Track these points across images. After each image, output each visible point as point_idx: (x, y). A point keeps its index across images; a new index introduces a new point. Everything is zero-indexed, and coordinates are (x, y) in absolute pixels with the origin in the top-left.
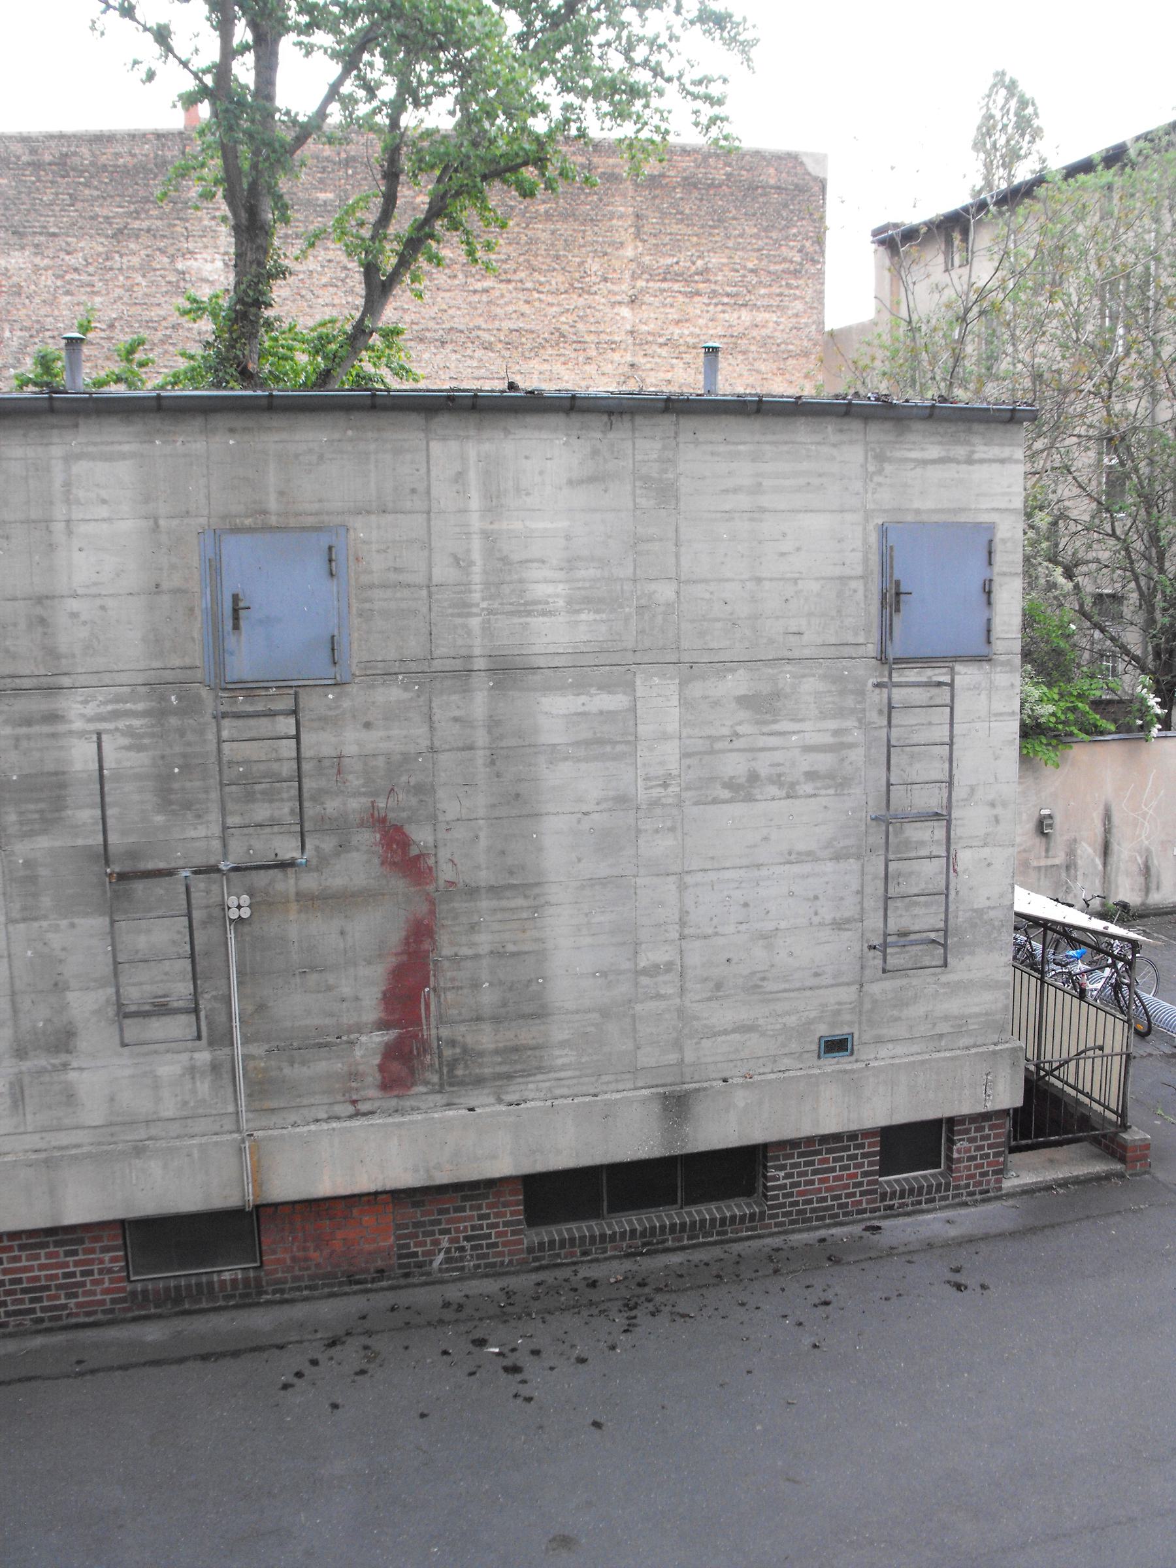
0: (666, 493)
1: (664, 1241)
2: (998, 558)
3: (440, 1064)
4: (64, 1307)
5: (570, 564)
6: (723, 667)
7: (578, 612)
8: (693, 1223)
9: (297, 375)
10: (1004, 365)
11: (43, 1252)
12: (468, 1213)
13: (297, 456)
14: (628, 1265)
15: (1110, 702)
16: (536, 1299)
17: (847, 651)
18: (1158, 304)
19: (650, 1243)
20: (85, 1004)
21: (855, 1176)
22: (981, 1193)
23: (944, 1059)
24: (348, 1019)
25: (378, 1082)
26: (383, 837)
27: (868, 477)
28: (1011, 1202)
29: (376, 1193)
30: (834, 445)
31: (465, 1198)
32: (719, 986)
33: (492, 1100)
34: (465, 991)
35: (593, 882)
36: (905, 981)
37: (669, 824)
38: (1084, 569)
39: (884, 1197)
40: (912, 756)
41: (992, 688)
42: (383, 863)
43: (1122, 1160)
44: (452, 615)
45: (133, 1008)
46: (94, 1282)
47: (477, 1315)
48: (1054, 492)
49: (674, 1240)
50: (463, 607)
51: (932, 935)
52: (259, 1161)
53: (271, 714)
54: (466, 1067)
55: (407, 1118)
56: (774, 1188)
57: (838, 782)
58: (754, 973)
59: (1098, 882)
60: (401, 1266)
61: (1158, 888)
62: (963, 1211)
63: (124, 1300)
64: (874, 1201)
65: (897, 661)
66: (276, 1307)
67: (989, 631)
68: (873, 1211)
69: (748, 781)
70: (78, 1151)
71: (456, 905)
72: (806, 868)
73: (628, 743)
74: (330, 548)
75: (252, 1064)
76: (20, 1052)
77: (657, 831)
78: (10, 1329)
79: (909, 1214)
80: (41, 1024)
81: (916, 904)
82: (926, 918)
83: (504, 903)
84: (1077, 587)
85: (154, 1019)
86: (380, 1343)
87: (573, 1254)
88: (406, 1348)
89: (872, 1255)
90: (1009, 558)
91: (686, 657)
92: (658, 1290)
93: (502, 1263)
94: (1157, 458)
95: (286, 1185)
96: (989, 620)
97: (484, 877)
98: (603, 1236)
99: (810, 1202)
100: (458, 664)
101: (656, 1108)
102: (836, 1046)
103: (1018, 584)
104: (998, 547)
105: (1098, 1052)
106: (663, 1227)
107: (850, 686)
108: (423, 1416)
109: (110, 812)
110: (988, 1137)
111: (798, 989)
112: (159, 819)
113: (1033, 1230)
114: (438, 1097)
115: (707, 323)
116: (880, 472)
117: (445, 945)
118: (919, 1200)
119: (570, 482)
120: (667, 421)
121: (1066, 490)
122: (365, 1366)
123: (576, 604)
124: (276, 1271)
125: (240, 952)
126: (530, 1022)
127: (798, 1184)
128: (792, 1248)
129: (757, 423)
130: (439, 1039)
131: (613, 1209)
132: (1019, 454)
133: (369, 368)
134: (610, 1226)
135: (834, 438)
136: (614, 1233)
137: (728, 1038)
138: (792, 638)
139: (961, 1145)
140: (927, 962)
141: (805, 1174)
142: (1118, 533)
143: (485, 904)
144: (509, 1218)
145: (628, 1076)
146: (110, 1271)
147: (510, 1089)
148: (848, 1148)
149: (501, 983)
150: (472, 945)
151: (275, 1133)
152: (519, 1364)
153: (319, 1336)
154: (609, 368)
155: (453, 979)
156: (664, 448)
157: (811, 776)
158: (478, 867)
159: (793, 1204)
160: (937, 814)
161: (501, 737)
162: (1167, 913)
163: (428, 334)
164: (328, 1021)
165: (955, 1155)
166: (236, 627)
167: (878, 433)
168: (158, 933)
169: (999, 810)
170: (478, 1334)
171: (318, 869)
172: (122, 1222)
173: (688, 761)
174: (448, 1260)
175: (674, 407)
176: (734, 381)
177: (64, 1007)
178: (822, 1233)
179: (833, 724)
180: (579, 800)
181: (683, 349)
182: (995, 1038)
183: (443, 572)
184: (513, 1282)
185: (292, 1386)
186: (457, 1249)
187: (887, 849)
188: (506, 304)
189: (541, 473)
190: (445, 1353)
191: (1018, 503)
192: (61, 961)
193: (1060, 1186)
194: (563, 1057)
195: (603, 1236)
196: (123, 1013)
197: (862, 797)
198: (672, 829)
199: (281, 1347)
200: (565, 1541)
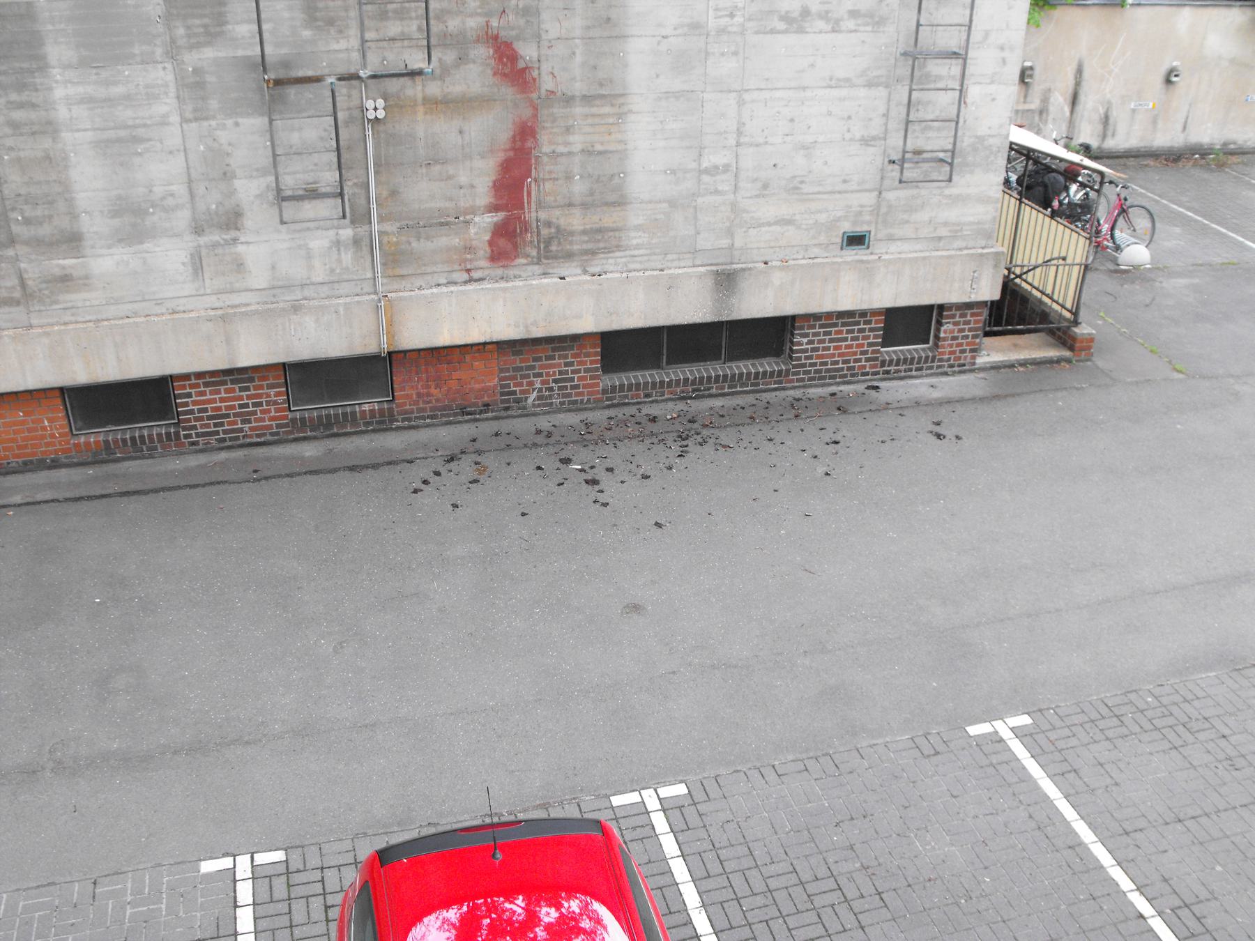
3: (539, 242)
4: (241, 430)
8: (733, 376)
11: (222, 388)
14: (681, 406)
19: (699, 390)
20: (250, 190)
21: (863, 345)
22: (959, 366)
25: (488, 255)
26: (496, 52)
28: (982, 375)
29: (485, 344)
32: (765, 186)
33: (579, 271)
34: (560, 182)
35: (668, 95)
36: (915, 192)
37: (733, 48)
39: (883, 364)
42: (495, 74)
43: (1071, 349)
45: (289, 193)
46: (263, 412)
47: (563, 440)
51: (941, 155)
55: (510, 284)
56: (798, 351)
57: (876, 20)
59: (1064, 127)
61: (1113, 135)
62: (944, 379)
63: (286, 425)
64: (875, 366)
66: (406, 432)
69: (801, 15)
70: (249, 308)
71: (555, 110)
72: (844, 92)
75: (385, 239)
76: (198, 230)
77: (723, 54)
78: (201, 446)
80: (214, 206)
81: (930, 128)
82: (937, 141)
83: (594, 110)
85: (306, 202)
86: (488, 460)
87: (638, 396)
89: (873, 408)
92: (705, 426)
93: (582, 400)
95: (414, 336)
97: (579, 88)
99: (825, 364)
101: (710, 282)
102: (856, 240)
105: (1061, 262)
109: (265, 27)
110: (968, 323)
112: (307, 34)
113: (997, 397)
114: (536, 267)
117: (546, 143)
118: (912, 367)
124: (404, 404)
125: (377, 146)
127: (816, 349)
130: (538, 221)
134: (668, 375)
139: (947, 327)
140: (935, 176)
141: (823, 341)
143: (579, 110)
146: (275, 403)
148: (858, 323)
149: (590, 176)
150: (567, 144)
151: (405, 294)
155: (550, 172)
158: (573, 79)
159: (812, 365)
160: (955, 53)
162: (1117, 157)
164: (448, 204)
165: (942, 335)
168: (308, 130)
169: (1006, 54)
170: (563, 455)
171: (441, 78)
172: (284, 364)
174: (539, 398)
177: (232, 193)
178: (833, 389)
180: (660, 25)
182: (983, 243)
184: (591, 416)
187: (912, 81)
190: (539, 468)
192: (228, 154)
193: (1021, 365)
194: (636, 238)
196: (282, 198)
197: (894, 35)
198: (735, 53)
199: (410, 462)
200: (636, 608)
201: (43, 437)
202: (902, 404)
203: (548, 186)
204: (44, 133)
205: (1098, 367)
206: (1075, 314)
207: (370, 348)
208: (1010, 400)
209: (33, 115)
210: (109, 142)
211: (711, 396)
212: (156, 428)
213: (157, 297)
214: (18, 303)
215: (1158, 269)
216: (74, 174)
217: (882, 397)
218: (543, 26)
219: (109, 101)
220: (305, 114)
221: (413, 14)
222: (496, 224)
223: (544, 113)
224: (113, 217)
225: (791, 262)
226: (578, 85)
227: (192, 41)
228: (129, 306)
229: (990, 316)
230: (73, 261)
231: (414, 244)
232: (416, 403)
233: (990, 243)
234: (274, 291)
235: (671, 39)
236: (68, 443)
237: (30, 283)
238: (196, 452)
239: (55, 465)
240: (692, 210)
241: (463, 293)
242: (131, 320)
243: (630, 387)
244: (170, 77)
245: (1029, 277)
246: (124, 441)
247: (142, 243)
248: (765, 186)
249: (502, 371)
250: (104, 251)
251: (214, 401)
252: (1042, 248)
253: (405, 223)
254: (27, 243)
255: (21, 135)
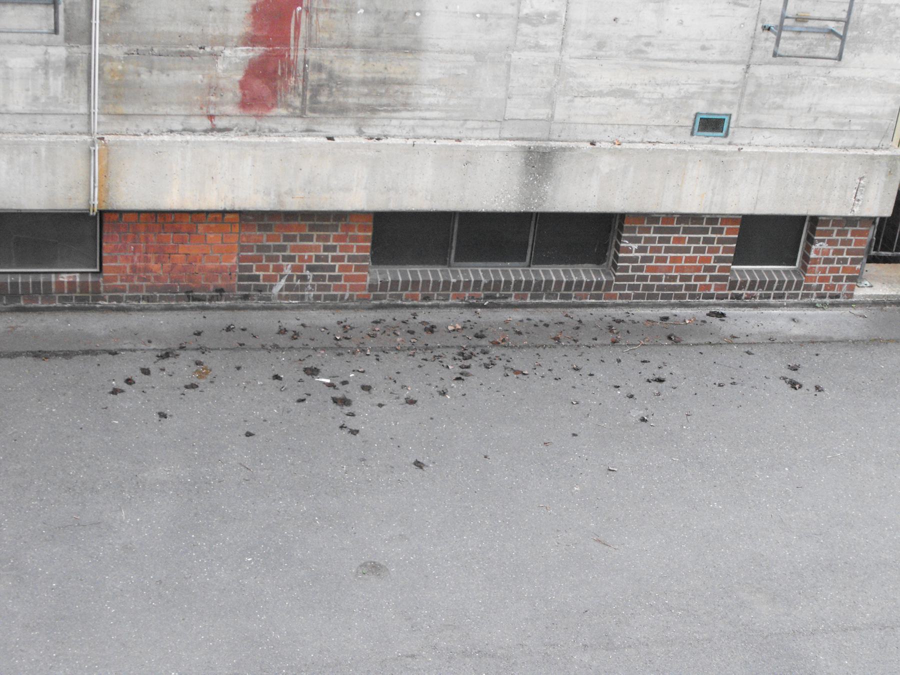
1: (506, 297)
3: (304, 88)
8: (539, 283)
12: (314, 243)
14: (468, 315)
16: (373, 336)
19: (493, 296)
21: (708, 259)
23: (821, 156)
24: (213, 30)
28: (859, 311)
29: (224, 212)
31: (312, 228)
32: (601, 45)
33: (352, 131)
34: (339, 15)
36: (793, 69)
39: (733, 285)
47: (312, 344)
49: (517, 297)
51: (832, 25)
52: (107, 167)
54: (331, 94)
55: (264, 139)
58: (639, 37)
60: (241, 288)
62: (810, 312)
64: (723, 288)
68: (720, 297)
75: (108, 66)
79: (755, 306)
86: (211, 361)
87: (414, 298)
88: (238, 368)
89: (713, 341)
92: (495, 344)
93: (342, 297)
95: (134, 192)
98: (447, 283)
99: (659, 279)
101: (518, 161)
102: (711, 125)
106: (508, 283)
108: (249, 434)
110: (849, 242)
111: (681, 61)
113: (876, 341)
118: (770, 293)
122: (195, 381)
124: (114, 279)
126: (402, 56)
127: (650, 259)
128: (634, 322)
130: (306, 62)
131: (460, 258)
134: (455, 273)
136: (459, 282)
137: (603, 100)
139: (820, 246)
141: (658, 250)
144: (355, 253)
145: (494, 125)
147: (371, 122)
148: (705, 231)
149: (377, 11)
152: (348, 397)
153: (152, 346)
164: (192, 29)
165: (813, 255)
170: (310, 363)
174: (288, 288)
178: (665, 312)
182: (876, 142)
185: (122, 391)
186: (298, 277)
190: (277, 377)
194: (429, 96)
195: (447, 283)
199: (113, 353)
200: (375, 568)
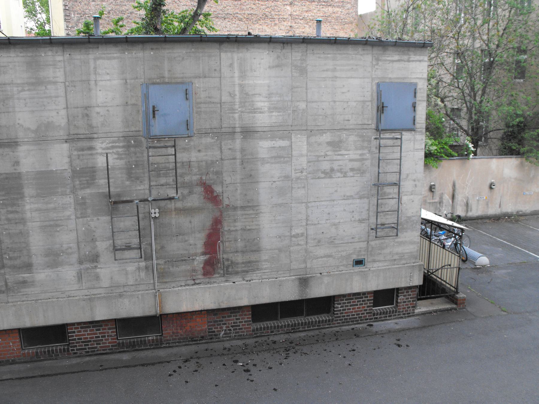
0: (303, 71)
2: (418, 95)
3: (224, 267)
4: (96, 348)
5: (270, 95)
6: (322, 132)
7: (272, 112)
9: (174, 30)
10: (421, 27)
11: (88, 329)
13: (175, 58)
14: (286, 336)
15: (456, 146)
17: (365, 127)
18: (476, 5)
19: (294, 329)
22: (407, 314)
26: (204, 189)
27: (373, 66)
28: (417, 317)
29: (201, 311)
30: (361, 55)
33: (241, 279)
34: (233, 242)
36: (383, 241)
37: (303, 186)
38: (448, 99)
40: (387, 163)
41: (415, 140)
43: (456, 304)
44: (229, 113)
45: (119, 247)
47: (235, 352)
48: (438, 72)
50: (232, 110)
51: (393, 225)
53: (166, 147)
55: (212, 285)
62: (401, 320)
64: (371, 316)
65: (382, 130)
67: (414, 120)
70: (100, 296)
72: (350, 201)
73: (289, 157)
74: (186, 90)
75: (159, 267)
77: (299, 188)
81: (387, 214)
82: (391, 219)
83: (246, 212)
84: (445, 105)
85: (126, 251)
87: (268, 332)
89: (370, 334)
90: (422, 95)
91: (309, 128)
92: (297, 345)
93: (244, 335)
94: (475, 60)
95: (171, 307)
96: (414, 117)
97: (239, 203)
99: (349, 316)
100: (231, 130)
101: (297, 283)
102: (359, 262)
103: (425, 104)
104: (418, 91)
105: (449, 267)
107: (366, 139)
109: (111, 181)
110: (410, 295)
112: (128, 183)
113: (424, 327)
115: (317, 12)
116: (377, 64)
117: (226, 226)
118: (387, 315)
119: (269, 67)
120: (303, 46)
121: (442, 71)
123: (271, 109)
127: (345, 310)
129: (335, 47)
132: (426, 58)
133: (199, 28)
134: (281, 323)
135: (361, 52)
138: (346, 122)
139: (401, 297)
140: (391, 234)
141: (347, 306)
142: (460, 87)
143: (239, 212)
146: (111, 336)
149: (245, 239)
151: (168, 290)
154: (282, 28)
156: (302, 55)
157: (352, 170)
158: (237, 200)
161: (245, 155)
163: (220, 16)
164: (185, 252)
165: (399, 301)
166: (154, 117)
167: (377, 51)
168: (127, 222)
169: (417, 183)
170: (235, 359)
171: (182, 200)
172: (115, 319)
173: (309, 164)
174: (225, 334)
175: (306, 41)
176: (327, 32)
178: (353, 326)
179: (360, 152)
181: (308, 21)
182: (414, 261)
183: (225, 98)
184: (248, 341)
188: (247, 5)
189: (259, 64)
190: (224, 365)
191: (425, 76)
193: (434, 312)
194: (265, 265)
196: (115, 249)
197: (369, 177)
198: (304, 187)
199: (168, 362)
201: (10, 350)
202: (383, 332)
203: (227, 244)
204: (20, 223)
205: (468, 312)
206: (457, 289)
207: (152, 312)
208: (430, 328)
209: (16, 216)
210: (46, 226)
211: (300, 331)
212: (59, 346)
213: (63, 290)
214: (4, 292)
215: (493, 266)
216: (31, 239)
217: (374, 329)
218: (224, 179)
219: (48, 210)
220: (126, 215)
221: (171, 175)
222: (205, 260)
223: (225, 214)
224: (45, 257)
225: (332, 273)
226: (239, 202)
227: (82, 186)
228: (50, 294)
229: (419, 291)
230: (28, 275)
231: (171, 269)
232: (172, 336)
233: (417, 261)
234: (112, 288)
235: (277, 182)
236: (20, 353)
237: (9, 284)
238: (76, 357)
239: (14, 362)
240: (288, 252)
241: (192, 289)
242: (51, 300)
243: (264, 328)
244: (72, 201)
245: (436, 273)
246: (45, 352)
247: (57, 268)
248: (319, 241)
249: (209, 322)
250: (41, 271)
251: (85, 335)
252: (441, 261)
253: (167, 260)
254: (10, 267)
255: (11, 224)
